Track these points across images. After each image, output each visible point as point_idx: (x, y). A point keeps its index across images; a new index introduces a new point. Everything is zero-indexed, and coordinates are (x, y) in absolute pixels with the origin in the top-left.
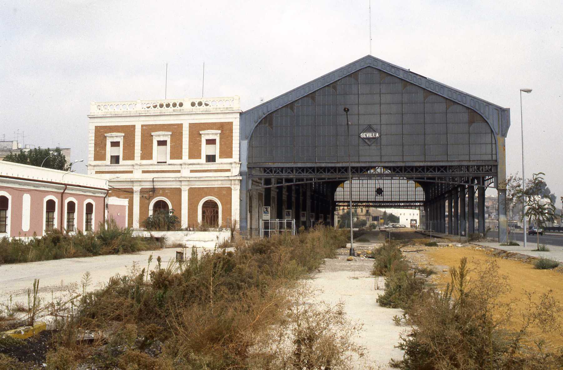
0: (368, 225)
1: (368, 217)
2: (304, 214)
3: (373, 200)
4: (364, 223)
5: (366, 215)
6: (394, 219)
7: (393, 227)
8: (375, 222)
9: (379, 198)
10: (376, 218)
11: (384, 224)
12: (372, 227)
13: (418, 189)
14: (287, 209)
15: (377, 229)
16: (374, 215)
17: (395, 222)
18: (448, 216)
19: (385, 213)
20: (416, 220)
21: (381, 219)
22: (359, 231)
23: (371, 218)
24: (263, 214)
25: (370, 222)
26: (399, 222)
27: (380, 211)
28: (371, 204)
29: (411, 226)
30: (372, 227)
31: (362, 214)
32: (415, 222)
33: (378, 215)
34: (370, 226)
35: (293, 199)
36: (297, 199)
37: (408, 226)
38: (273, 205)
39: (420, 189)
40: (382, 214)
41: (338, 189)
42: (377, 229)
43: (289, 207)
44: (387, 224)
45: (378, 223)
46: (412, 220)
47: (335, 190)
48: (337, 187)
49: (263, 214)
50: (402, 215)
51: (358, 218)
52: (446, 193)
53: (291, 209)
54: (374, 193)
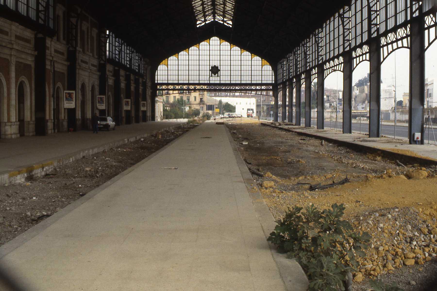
0: (201, 115)
1: (201, 106)
2: (70, 95)
3: (206, 82)
4: (197, 113)
5: (199, 104)
6: (230, 108)
7: (230, 117)
8: (210, 112)
9: (215, 80)
10: (210, 107)
11: (220, 113)
12: (206, 118)
13: (265, 67)
14: (68, 89)
15: (212, 120)
16: (208, 104)
17: (231, 111)
18: (288, 106)
19: (220, 102)
20: (252, 110)
21: (216, 108)
22: (188, 123)
23: (205, 107)
24: (65, 102)
25: (204, 111)
26: (235, 112)
27: (216, 100)
28: (205, 87)
29: (248, 116)
30: (206, 118)
31: (195, 103)
32: (251, 111)
33: (213, 104)
34: (204, 116)
35: (123, 85)
36: (137, 88)
37: (245, 115)
38: (110, 93)
39: (268, 68)
40: (217, 103)
41: (160, 67)
42: (212, 120)
43: (128, 97)
44: (223, 114)
45: (213, 113)
46: (248, 110)
47: (157, 69)
48: (159, 64)
49: (65, 102)
50: (239, 103)
51: (190, 107)
52: (280, 84)
53: (74, 88)
54: (208, 73)
